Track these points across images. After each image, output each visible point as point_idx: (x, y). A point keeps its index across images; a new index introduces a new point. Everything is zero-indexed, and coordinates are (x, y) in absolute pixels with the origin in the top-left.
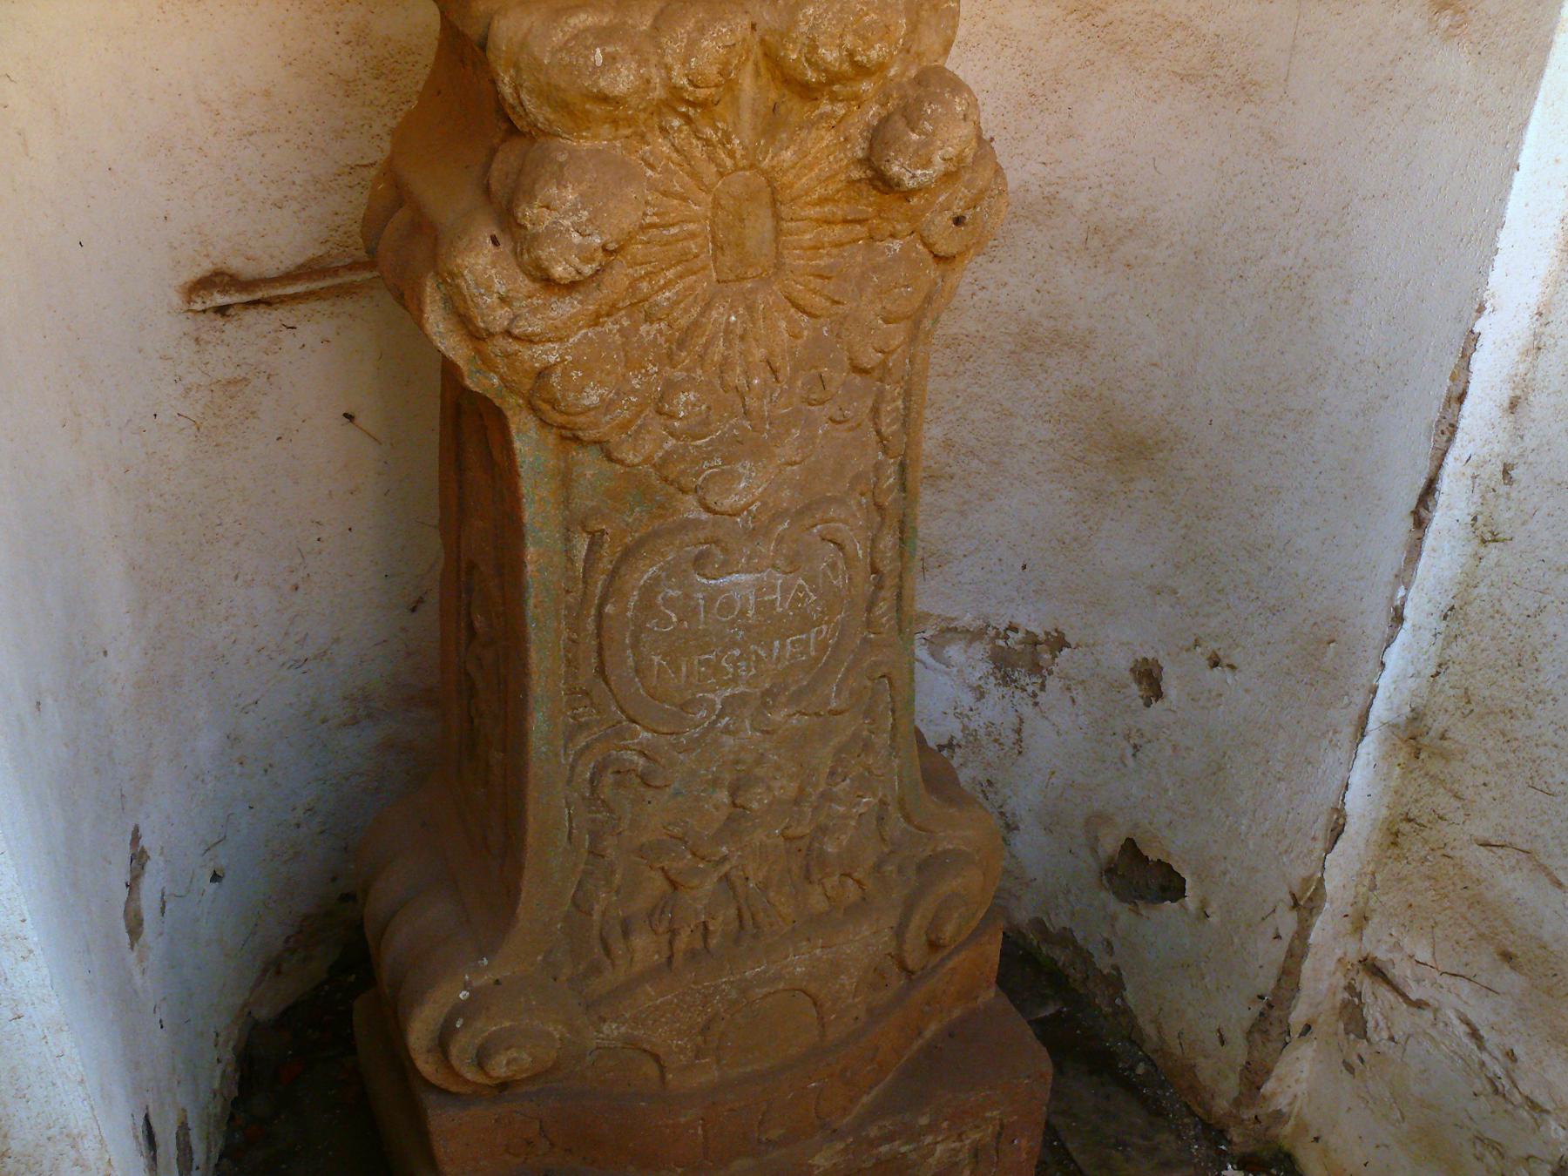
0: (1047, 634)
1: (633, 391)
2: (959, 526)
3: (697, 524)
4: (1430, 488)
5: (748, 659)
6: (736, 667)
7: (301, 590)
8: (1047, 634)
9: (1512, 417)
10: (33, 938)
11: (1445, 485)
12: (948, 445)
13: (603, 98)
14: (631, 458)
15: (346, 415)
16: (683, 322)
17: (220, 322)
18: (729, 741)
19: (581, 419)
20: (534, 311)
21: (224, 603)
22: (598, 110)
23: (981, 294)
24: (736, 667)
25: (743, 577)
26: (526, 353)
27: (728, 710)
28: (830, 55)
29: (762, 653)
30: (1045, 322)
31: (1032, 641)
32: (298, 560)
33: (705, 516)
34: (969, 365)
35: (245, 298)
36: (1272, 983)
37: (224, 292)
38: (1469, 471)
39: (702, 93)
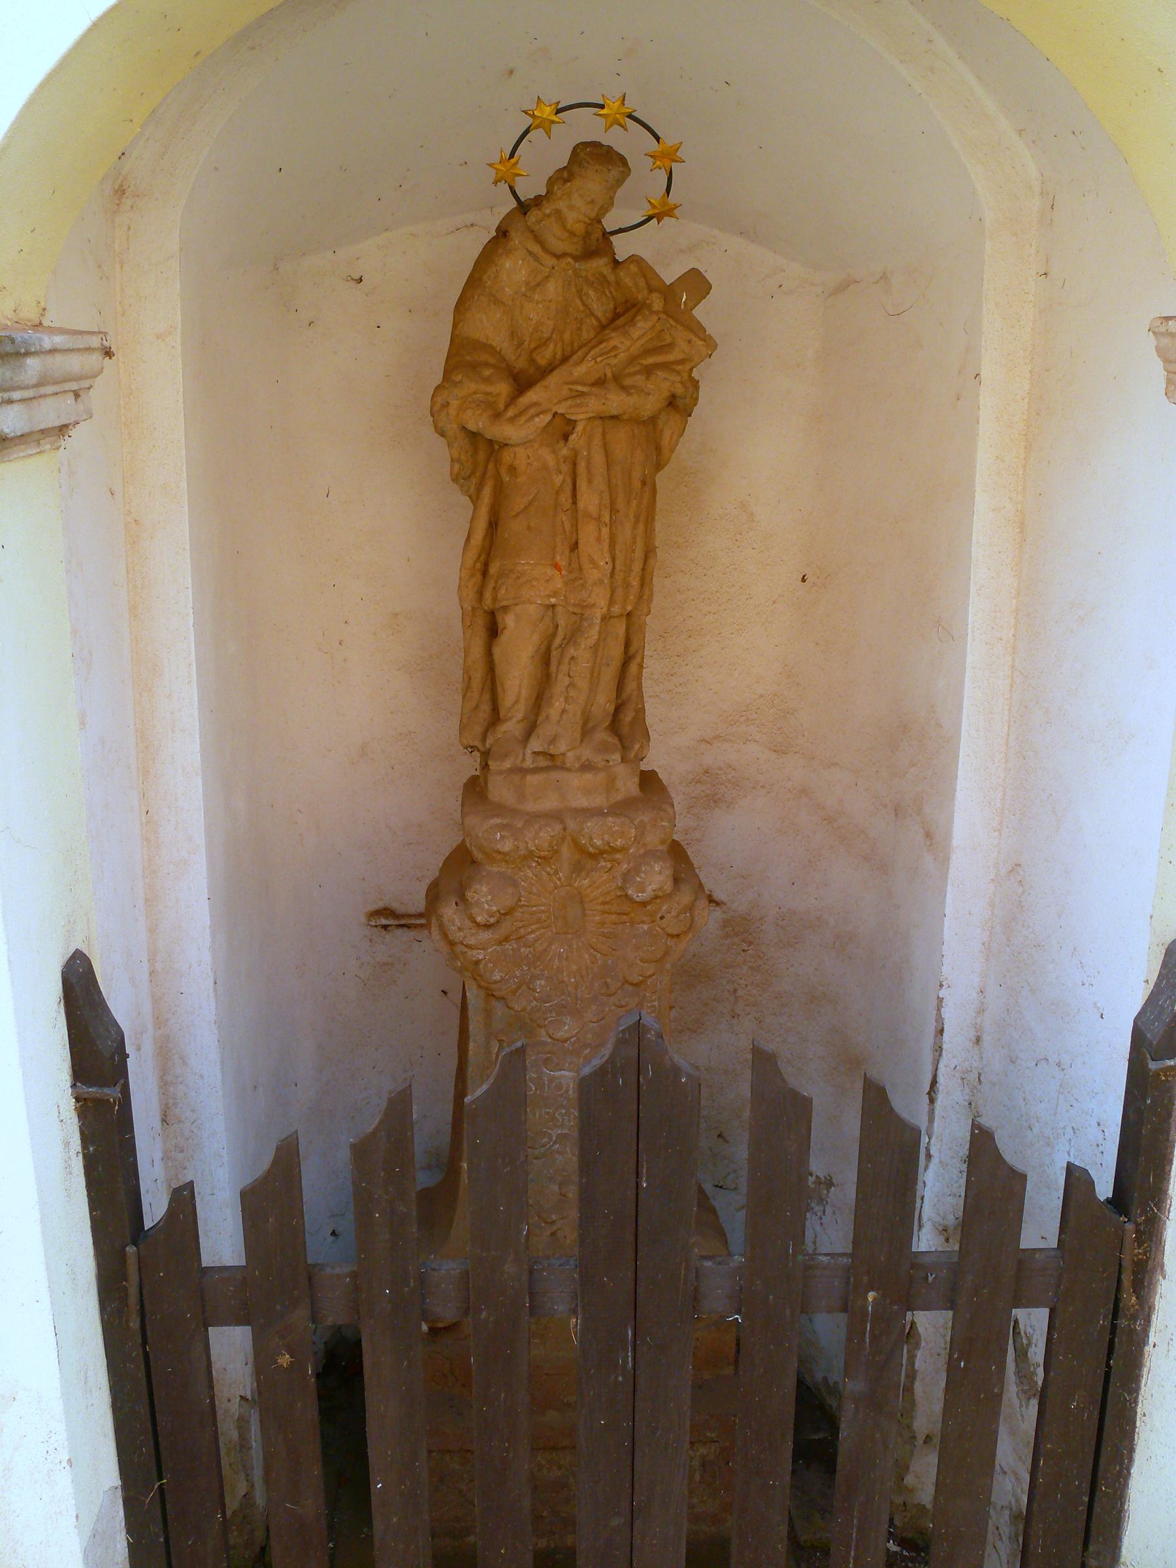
1: (516, 976)
3: (545, 1043)
4: (934, 1082)
9: (976, 1048)
10: (226, 1159)
11: (941, 1079)
13: (499, 852)
14: (516, 1007)
16: (540, 949)
17: (384, 933)
18: (559, 1158)
19: (493, 986)
20: (472, 935)
22: (499, 857)
25: (567, 1073)
26: (470, 953)
28: (598, 842)
33: (549, 1040)
35: (396, 922)
36: (939, 1425)
37: (386, 918)
38: (958, 1075)
39: (543, 854)
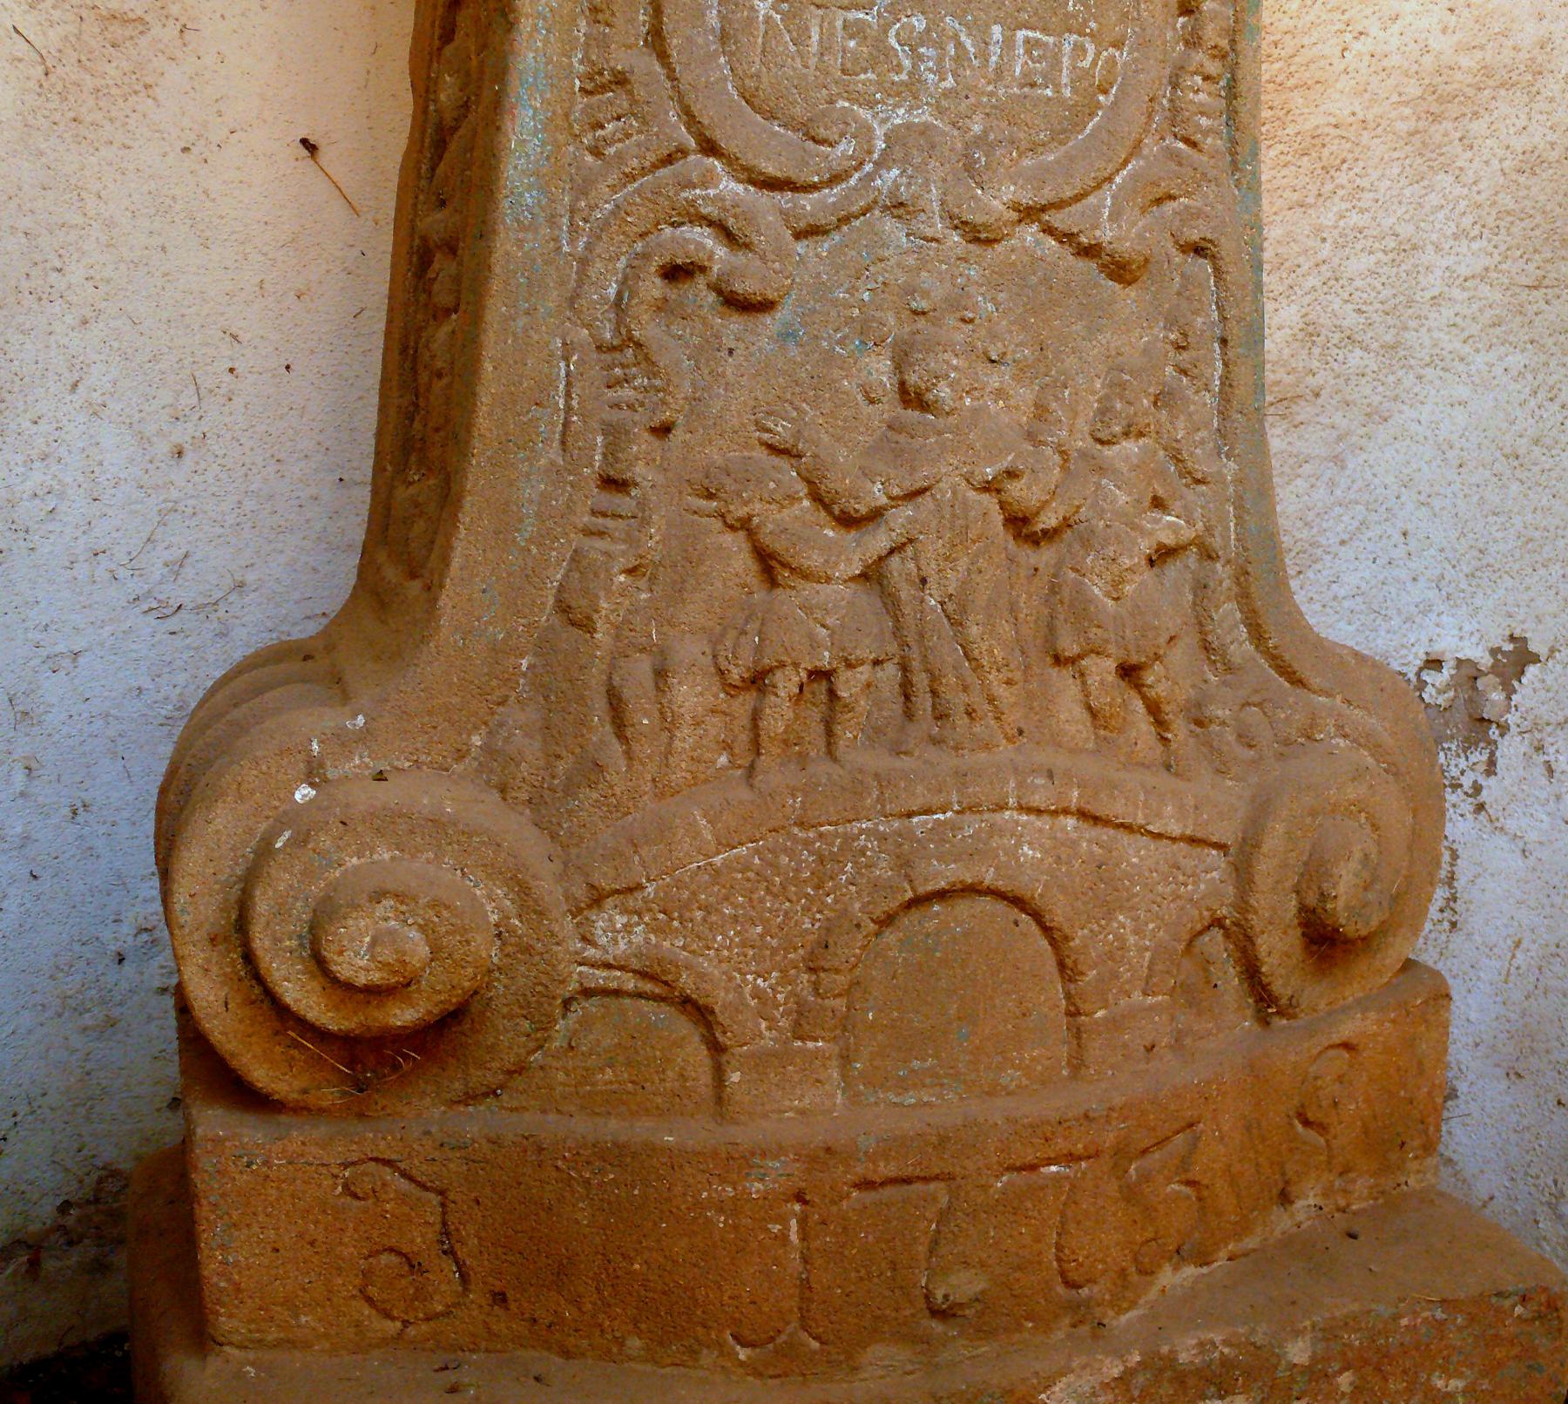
0: (1494, 652)
2: (1332, 484)
5: (941, 47)
6: (918, 58)
7: (188, 459)
8: (1494, 652)
12: (1309, 332)
15: (304, 142)
21: (43, 427)
23: (1357, 46)
24: (918, 58)
27: (898, 153)
29: (968, 43)
30: (1465, 61)
31: (1469, 674)
32: (188, 399)
34: (1342, 178)
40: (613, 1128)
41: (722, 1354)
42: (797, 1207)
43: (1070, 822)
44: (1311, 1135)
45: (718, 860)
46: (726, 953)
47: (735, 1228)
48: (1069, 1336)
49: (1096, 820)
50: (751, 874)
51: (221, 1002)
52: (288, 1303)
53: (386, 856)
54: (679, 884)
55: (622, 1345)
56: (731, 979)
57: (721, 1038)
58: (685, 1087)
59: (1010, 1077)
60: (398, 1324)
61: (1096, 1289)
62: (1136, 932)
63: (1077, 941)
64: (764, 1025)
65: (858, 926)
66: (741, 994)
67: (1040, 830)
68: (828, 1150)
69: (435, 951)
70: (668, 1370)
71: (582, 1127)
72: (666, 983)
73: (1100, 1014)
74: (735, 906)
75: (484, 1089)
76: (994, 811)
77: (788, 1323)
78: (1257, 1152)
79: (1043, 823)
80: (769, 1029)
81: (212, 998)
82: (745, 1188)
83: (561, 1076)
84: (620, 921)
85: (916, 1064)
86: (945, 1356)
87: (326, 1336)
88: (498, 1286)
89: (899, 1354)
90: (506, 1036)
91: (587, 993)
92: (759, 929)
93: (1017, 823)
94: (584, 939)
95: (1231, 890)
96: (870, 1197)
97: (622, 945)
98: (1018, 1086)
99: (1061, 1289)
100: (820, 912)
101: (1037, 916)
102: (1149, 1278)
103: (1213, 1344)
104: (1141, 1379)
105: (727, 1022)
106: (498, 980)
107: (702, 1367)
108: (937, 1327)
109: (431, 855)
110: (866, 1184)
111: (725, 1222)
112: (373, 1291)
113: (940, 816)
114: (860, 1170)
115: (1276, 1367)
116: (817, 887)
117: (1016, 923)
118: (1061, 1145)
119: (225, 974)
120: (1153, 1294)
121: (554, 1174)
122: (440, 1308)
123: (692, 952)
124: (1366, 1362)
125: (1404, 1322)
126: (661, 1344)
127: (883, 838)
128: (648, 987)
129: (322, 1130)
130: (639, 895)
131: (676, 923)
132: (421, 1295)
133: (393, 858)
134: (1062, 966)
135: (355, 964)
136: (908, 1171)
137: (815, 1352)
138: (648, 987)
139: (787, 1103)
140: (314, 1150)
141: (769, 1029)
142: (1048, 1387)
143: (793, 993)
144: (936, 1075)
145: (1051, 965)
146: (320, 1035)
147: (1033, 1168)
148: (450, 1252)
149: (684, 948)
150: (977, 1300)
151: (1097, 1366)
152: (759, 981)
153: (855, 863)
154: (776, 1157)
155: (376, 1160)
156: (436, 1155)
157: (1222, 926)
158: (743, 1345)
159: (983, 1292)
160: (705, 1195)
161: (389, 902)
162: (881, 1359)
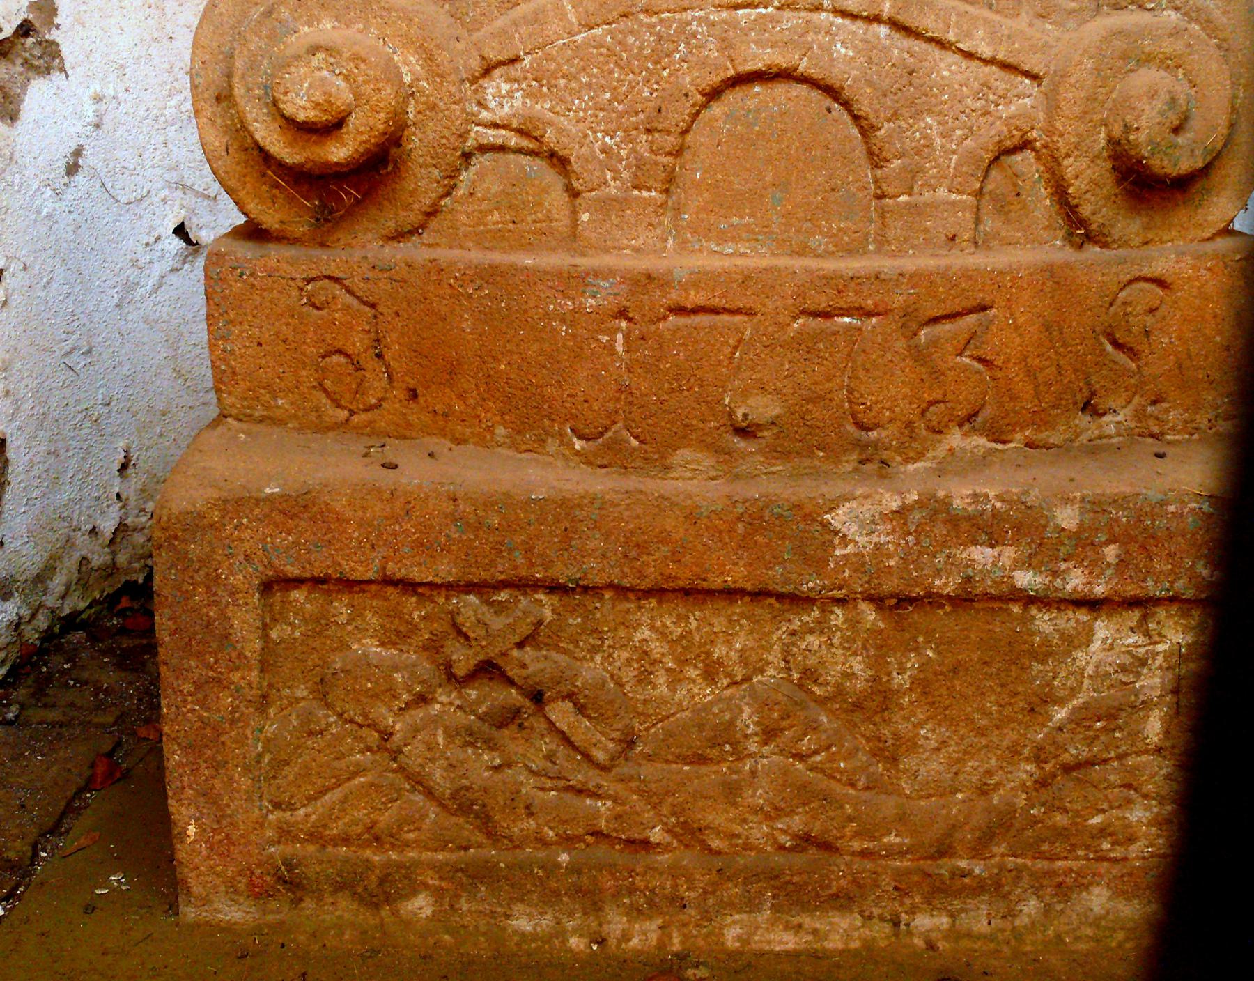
40: (497, 257)
41: (562, 443)
42: (624, 324)
43: (883, 30)
44: (1122, 357)
45: (579, 38)
46: (581, 114)
47: (574, 336)
48: (856, 470)
49: (907, 31)
50: (604, 50)
51: (223, 147)
52: (267, 387)
53: (329, 26)
54: (549, 58)
55: (493, 433)
56: (586, 136)
57: (575, 184)
58: (551, 227)
59: (817, 241)
60: (346, 413)
61: (884, 433)
62: (942, 135)
63: (883, 131)
64: (609, 175)
65: (686, 95)
66: (592, 148)
67: (854, 33)
68: (649, 277)
69: (357, 97)
70: (524, 455)
71: (476, 256)
72: (536, 138)
73: (904, 198)
74: (591, 75)
75: (409, 227)
76: (810, 11)
77: (614, 423)
78: (1057, 353)
79: (858, 27)
80: (614, 179)
81: (217, 144)
82: (581, 303)
83: (464, 219)
84: (505, 87)
85: (735, 220)
86: (744, 467)
87: (295, 416)
88: (413, 383)
89: (706, 461)
90: (421, 180)
91: (484, 149)
92: (608, 95)
93: (832, 24)
94: (479, 104)
95: (1041, 116)
96: (683, 321)
97: (506, 109)
98: (825, 251)
99: (851, 428)
100: (657, 83)
101: (846, 105)
102: (938, 437)
103: (987, 496)
104: (917, 515)
105: (578, 170)
106: (414, 134)
107: (547, 454)
108: (740, 443)
109: (361, 26)
110: (680, 310)
111: (566, 331)
112: (328, 384)
113: (763, 11)
114: (675, 296)
115: (1045, 527)
116: (656, 63)
117: (829, 110)
118: (851, 298)
119: (226, 126)
120: (941, 451)
121: (449, 291)
122: (374, 401)
123: (557, 113)
124: (1133, 539)
125: (1172, 508)
126: (519, 432)
127: (713, 24)
128: (525, 143)
129: (289, 252)
130: (518, 66)
131: (545, 89)
132: (360, 390)
133: (333, 28)
134: (870, 153)
135: (301, 106)
136: (715, 302)
137: (634, 449)
138: (525, 143)
139: (625, 242)
140: (285, 266)
141: (614, 179)
142: (832, 509)
143: (634, 150)
144: (752, 232)
145: (860, 152)
146: (281, 165)
147: (827, 315)
148: (379, 356)
149: (550, 110)
150: (773, 423)
151: (878, 497)
152: (607, 139)
153: (688, 44)
154: (604, 279)
155: (329, 278)
156: (370, 275)
157: (1033, 149)
158: (580, 437)
159: (778, 417)
160: (552, 307)
161: (321, 55)
162: (688, 462)
